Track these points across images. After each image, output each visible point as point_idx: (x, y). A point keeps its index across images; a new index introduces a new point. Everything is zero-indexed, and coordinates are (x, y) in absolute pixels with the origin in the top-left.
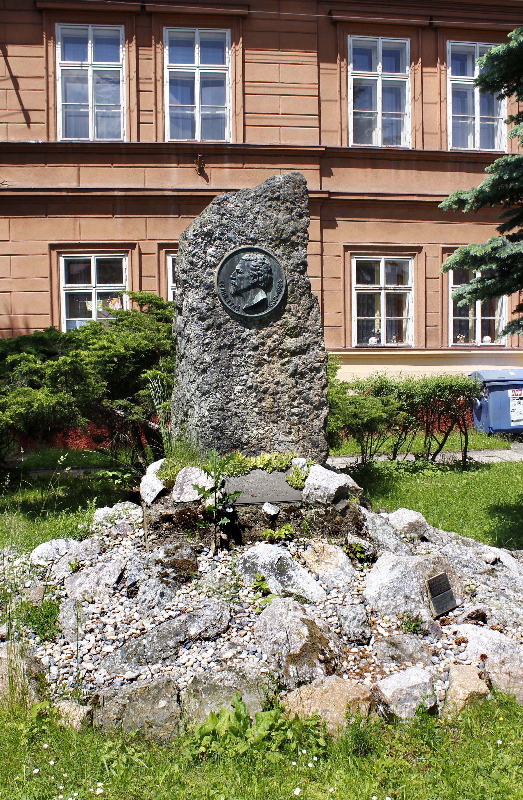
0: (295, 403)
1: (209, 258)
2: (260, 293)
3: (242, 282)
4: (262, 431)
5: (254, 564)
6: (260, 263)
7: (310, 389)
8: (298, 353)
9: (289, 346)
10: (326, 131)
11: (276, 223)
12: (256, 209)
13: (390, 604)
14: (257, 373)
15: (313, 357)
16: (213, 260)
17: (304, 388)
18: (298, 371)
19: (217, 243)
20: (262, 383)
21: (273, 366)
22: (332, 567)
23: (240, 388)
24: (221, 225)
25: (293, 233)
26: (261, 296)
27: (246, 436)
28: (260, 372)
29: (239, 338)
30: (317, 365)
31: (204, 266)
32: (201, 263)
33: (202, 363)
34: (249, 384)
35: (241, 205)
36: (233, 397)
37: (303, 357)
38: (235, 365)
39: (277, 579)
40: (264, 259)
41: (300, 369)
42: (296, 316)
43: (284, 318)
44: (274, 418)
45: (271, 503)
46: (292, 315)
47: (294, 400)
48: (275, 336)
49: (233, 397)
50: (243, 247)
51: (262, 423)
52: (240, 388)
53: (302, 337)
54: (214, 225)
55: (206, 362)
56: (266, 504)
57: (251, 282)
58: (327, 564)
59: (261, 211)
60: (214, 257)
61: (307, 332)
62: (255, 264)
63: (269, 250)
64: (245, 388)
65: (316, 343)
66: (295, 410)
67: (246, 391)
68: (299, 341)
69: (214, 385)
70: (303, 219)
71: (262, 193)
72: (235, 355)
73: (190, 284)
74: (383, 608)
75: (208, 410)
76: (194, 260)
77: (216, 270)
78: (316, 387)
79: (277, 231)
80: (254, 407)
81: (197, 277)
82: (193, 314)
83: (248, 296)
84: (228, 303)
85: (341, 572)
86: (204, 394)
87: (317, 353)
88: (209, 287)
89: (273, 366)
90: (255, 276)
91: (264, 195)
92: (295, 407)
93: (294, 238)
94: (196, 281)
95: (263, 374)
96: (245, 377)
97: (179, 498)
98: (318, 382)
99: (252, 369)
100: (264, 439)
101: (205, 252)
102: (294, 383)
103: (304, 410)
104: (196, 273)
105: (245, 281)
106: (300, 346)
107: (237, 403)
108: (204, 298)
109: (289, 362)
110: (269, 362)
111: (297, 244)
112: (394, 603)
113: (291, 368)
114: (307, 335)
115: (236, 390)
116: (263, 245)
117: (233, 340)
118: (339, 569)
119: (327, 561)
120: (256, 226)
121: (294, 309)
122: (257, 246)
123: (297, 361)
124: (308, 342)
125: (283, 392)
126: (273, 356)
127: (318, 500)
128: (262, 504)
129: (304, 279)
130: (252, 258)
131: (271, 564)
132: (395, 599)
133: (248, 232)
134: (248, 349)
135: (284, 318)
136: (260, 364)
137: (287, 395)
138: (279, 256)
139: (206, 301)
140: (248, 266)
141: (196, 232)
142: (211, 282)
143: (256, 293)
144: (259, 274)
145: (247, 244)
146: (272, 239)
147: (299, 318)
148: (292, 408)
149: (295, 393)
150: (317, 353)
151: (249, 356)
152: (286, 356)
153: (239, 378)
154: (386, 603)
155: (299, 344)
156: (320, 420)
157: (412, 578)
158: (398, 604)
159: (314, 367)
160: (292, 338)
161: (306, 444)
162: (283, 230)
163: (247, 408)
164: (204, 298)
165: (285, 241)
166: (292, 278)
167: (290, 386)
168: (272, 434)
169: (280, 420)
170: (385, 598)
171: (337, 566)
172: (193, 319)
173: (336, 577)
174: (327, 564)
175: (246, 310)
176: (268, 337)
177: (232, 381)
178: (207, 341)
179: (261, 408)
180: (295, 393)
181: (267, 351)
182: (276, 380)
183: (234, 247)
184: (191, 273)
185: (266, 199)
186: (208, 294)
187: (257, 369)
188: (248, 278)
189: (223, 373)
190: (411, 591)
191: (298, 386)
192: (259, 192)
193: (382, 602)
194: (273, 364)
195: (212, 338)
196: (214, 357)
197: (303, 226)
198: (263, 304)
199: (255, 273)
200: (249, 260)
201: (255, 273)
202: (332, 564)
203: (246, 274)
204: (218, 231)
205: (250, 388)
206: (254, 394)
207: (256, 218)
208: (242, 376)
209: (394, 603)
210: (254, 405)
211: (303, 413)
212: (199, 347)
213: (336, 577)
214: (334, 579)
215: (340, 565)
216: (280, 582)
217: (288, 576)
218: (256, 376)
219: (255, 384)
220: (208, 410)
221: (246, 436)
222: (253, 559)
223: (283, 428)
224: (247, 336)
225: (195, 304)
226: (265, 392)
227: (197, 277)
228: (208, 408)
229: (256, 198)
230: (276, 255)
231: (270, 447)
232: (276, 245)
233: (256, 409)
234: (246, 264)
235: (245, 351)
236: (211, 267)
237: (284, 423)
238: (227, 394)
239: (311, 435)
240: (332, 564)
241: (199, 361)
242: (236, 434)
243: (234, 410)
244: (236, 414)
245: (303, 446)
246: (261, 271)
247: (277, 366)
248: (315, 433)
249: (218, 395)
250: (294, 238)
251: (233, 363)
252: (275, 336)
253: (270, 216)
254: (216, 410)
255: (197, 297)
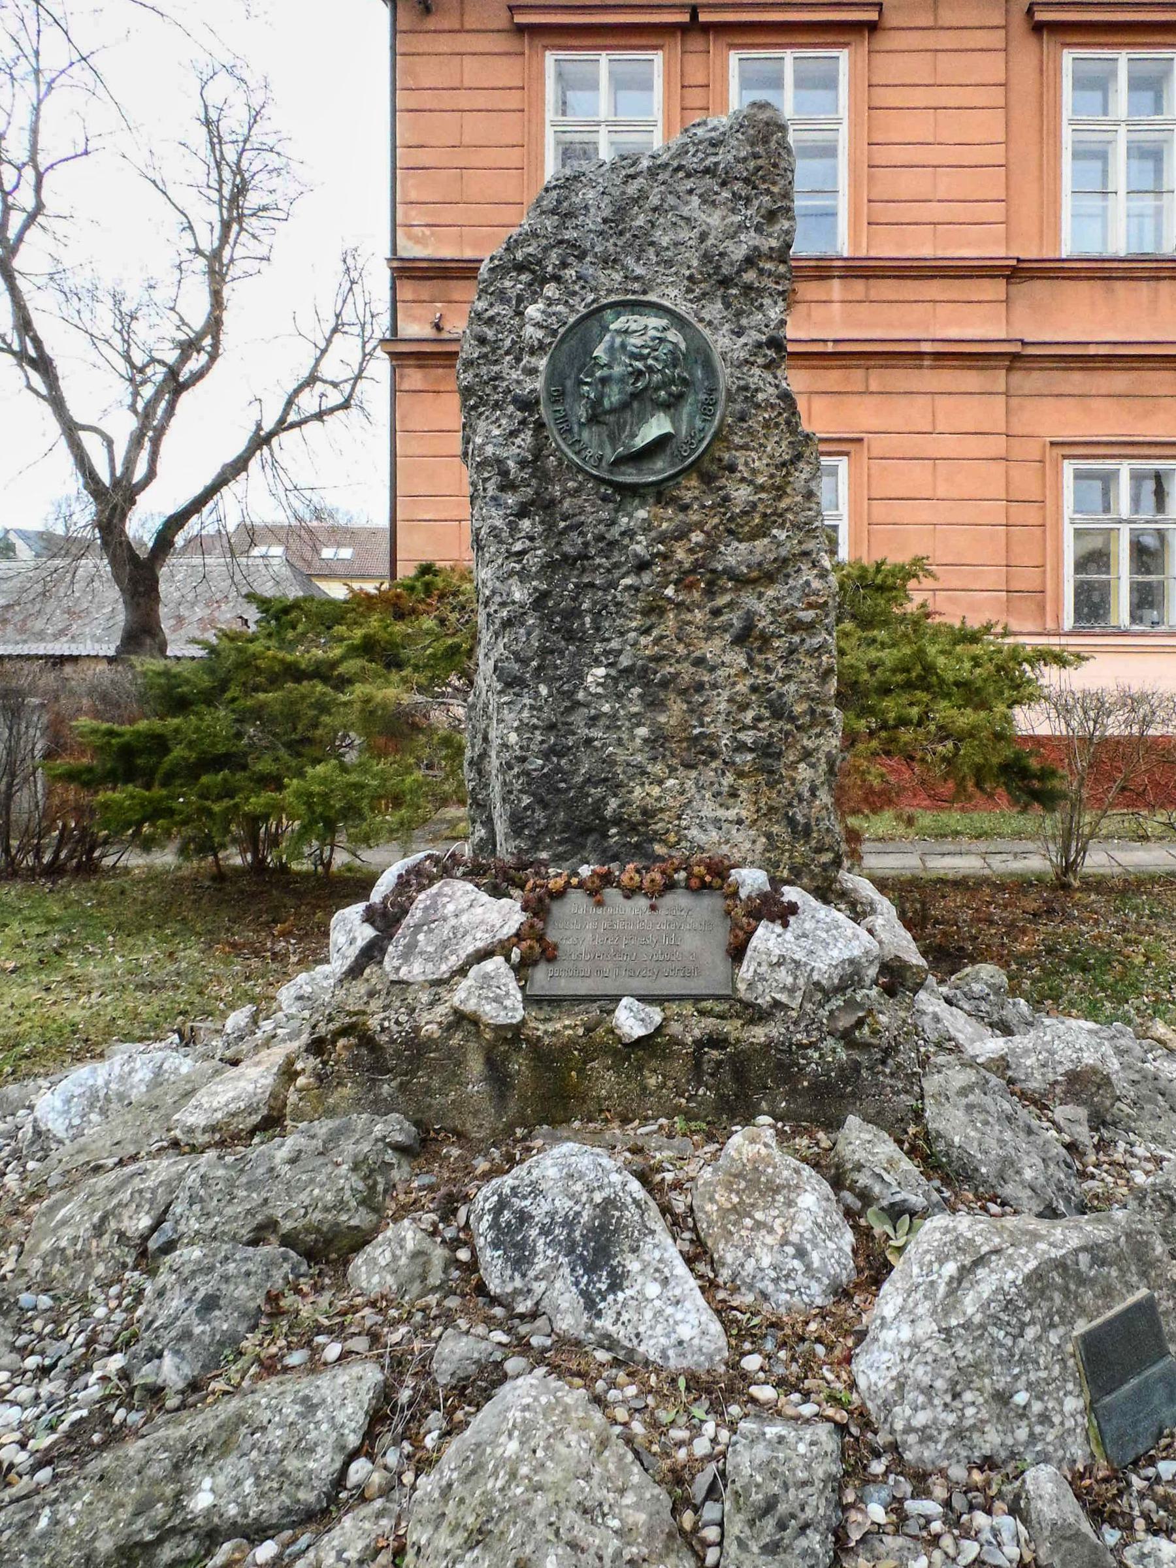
0: (749, 716)
1: (529, 330)
2: (653, 421)
3: (607, 390)
4: (656, 791)
5: (524, 1217)
6: (653, 339)
7: (786, 679)
8: (754, 582)
9: (732, 561)
10: (935, 174)
11: (703, 237)
12: (654, 200)
13: (935, 1421)
14: (647, 631)
15: (797, 595)
16: (540, 334)
17: (772, 677)
18: (757, 632)
19: (550, 290)
20: (658, 659)
21: (689, 617)
22: (769, 1240)
23: (601, 671)
24: (561, 242)
25: (750, 261)
26: (656, 427)
27: (613, 803)
28: (655, 633)
29: (600, 538)
30: (808, 615)
31: (518, 351)
32: (508, 343)
33: (503, 604)
34: (625, 661)
35: (616, 192)
36: (581, 695)
37: (771, 593)
38: (590, 611)
39: (577, 1284)
40: (665, 329)
41: (760, 625)
42: (751, 483)
43: (721, 488)
44: (688, 756)
45: (641, 999)
46: (743, 480)
47: (743, 707)
48: (697, 537)
49: (581, 695)
50: (614, 298)
51: (657, 769)
52: (601, 671)
53: (766, 541)
54: (544, 242)
55: (514, 603)
56: (625, 1001)
57: (630, 389)
58: (759, 1225)
59: (666, 206)
60: (541, 327)
61: (782, 526)
62: (638, 341)
63: (683, 308)
64: (613, 672)
65: (806, 554)
66: (747, 737)
67: (615, 680)
68: (759, 550)
69: (534, 663)
70: (777, 227)
71: (672, 158)
72: (591, 585)
73: (481, 398)
74: (912, 1439)
75: (517, 729)
76: (490, 334)
77: (542, 363)
78: (804, 676)
79: (705, 255)
80: (638, 725)
81: (495, 379)
82: (486, 475)
83: (621, 428)
84: (570, 446)
85: (796, 1264)
86: (509, 685)
87: (808, 583)
88: (527, 404)
89: (689, 617)
90: (639, 374)
91: (675, 164)
92: (745, 728)
93: (750, 276)
94: (495, 388)
95: (662, 637)
96: (614, 644)
97: (398, 969)
98: (808, 662)
99: (634, 624)
100: (662, 810)
101: (520, 314)
102: (745, 664)
103: (771, 735)
104: (496, 368)
105: (615, 389)
106: (760, 564)
107: (593, 711)
108: (513, 434)
109: (731, 605)
110: (679, 606)
111: (760, 292)
112: (951, 1419)
113: (735, 618)
114: (782, 535)
115: (590, 679)
116: (671, 296)
117: (586, 544)
118: (790, 1250)
119: (759, 1216)
120: (652, 244)
121: (746, 464)
122: (652, 297)
123: (754, 603)
124: (783, 552)
125: (714, 686)
126: (690, 587)
127: (778, 996)
128: (616, 999)
129: (777, 386)
130: (634, 326)
131: (569, 1223)
132: (957, 1404)
133: (630, 261)
134: (625, 569)
135: (721, 488)
136: (655, 610)
137: (725, 695)
138: (710, 323)
139: (518, 441)
140: (623, 346)
141: (496, 262)
142: (532, 391)
143: (642, 420)
144: (650, 369)
145: (627, 291)
146: (691, 278)
147: (762, 488)
148: (739, 730)
149: (745, 690)
150: (808, 583)
151: (628, 588)
152: (724, 590)
153: (598, 648)
154: (921, 1419)
155: (757, 558)
156: (812, 766)
157: (1023, 1326)
158: (968, 1423)
159: (800, 621)
160: (740, 541)
161: (775, 829)
162: (721, 255)
163: (619, 728)
164: (513, 434)
165: (725, 282)
166: (742, 383)
167: (733, 671)
168: (683, 799)
169: (705, 764)
170: (921, 1399)
171: (785, 1242)
172: (485, 490)
173: (776, 1281)
174: (759, 1225)
175: (620, 461)
176: (677, 539)
177: (580, 653)
178: (518, 547)
179: (657, 729)
180: (745, 690)
181: (674, 576)
182: (697, 654)
183: (594, 301)
184: (484, 370)
185: (681, 174)
186: (523, 422)
187: (649, 623)
188: (622, 380)
189: (557, 630)
190: (1016, 1377)
191: (755, 672)
192: (665, 157)
193: (908, 1412)
194: (689, 610)
195: (532, 539)
196: (536, 589)
197: (774, 243)
198: (661, 443)
199: (639, 365)
200: (626, 332)
201: (639, 365)
202: (771, 1231)
203: (617, 370)
204: (554, 257)
205: (628, 671)
206: (637, 690)
207: (653, 224)
208: (608, 640)
209: (951, 1419)
210: (637, 720)
211: (769, 745)
212: (500, 561)
213: (776, 1281)
214: (770, 1288)
215: (794, 1238)
216: (584, 1293)
217: (612, 1274)
218: (643, 640)
219: (640, 662)
220: (517, 729)
221: (613, 803)
222: (525, 1198)
223: (712, 784)
224: (623, 534)
225: (489, 450)
226: (664, 684)
227: (495, 379)
228: (516, 724)
229: (652, 172)
230: (701, 320)
231: (677, 833)
232: (704, 294)
233: (643, 731)
234: (618, 340)
235: (617, 574)
236: (532, 353)
237: (716, 770)
238: (566, 688)
239: (790, 805)
240: (771, 1231)
241: (497, 599)
242: (588, 795)
243: (584, 732)
244: (589, 741)
245: (769, 836)
246: (656, 359)
247: (699, 616)
248: (801, 800)
249: (544, 690)
250: (750, 276)
251: (585, 606)
252: (697, 537)
253: (687, 220)
254: (535, 727)
255: (496, 432)
